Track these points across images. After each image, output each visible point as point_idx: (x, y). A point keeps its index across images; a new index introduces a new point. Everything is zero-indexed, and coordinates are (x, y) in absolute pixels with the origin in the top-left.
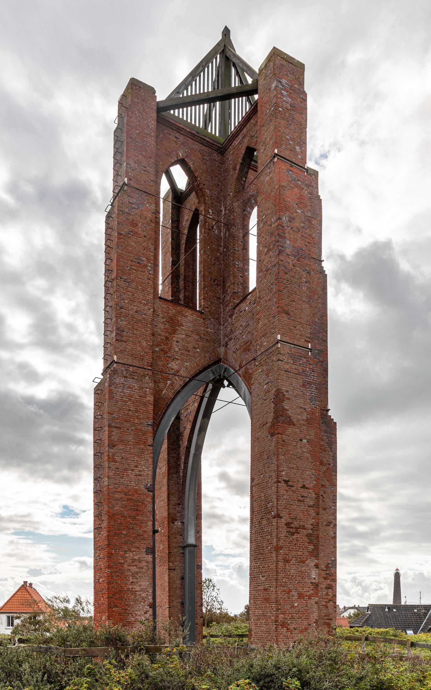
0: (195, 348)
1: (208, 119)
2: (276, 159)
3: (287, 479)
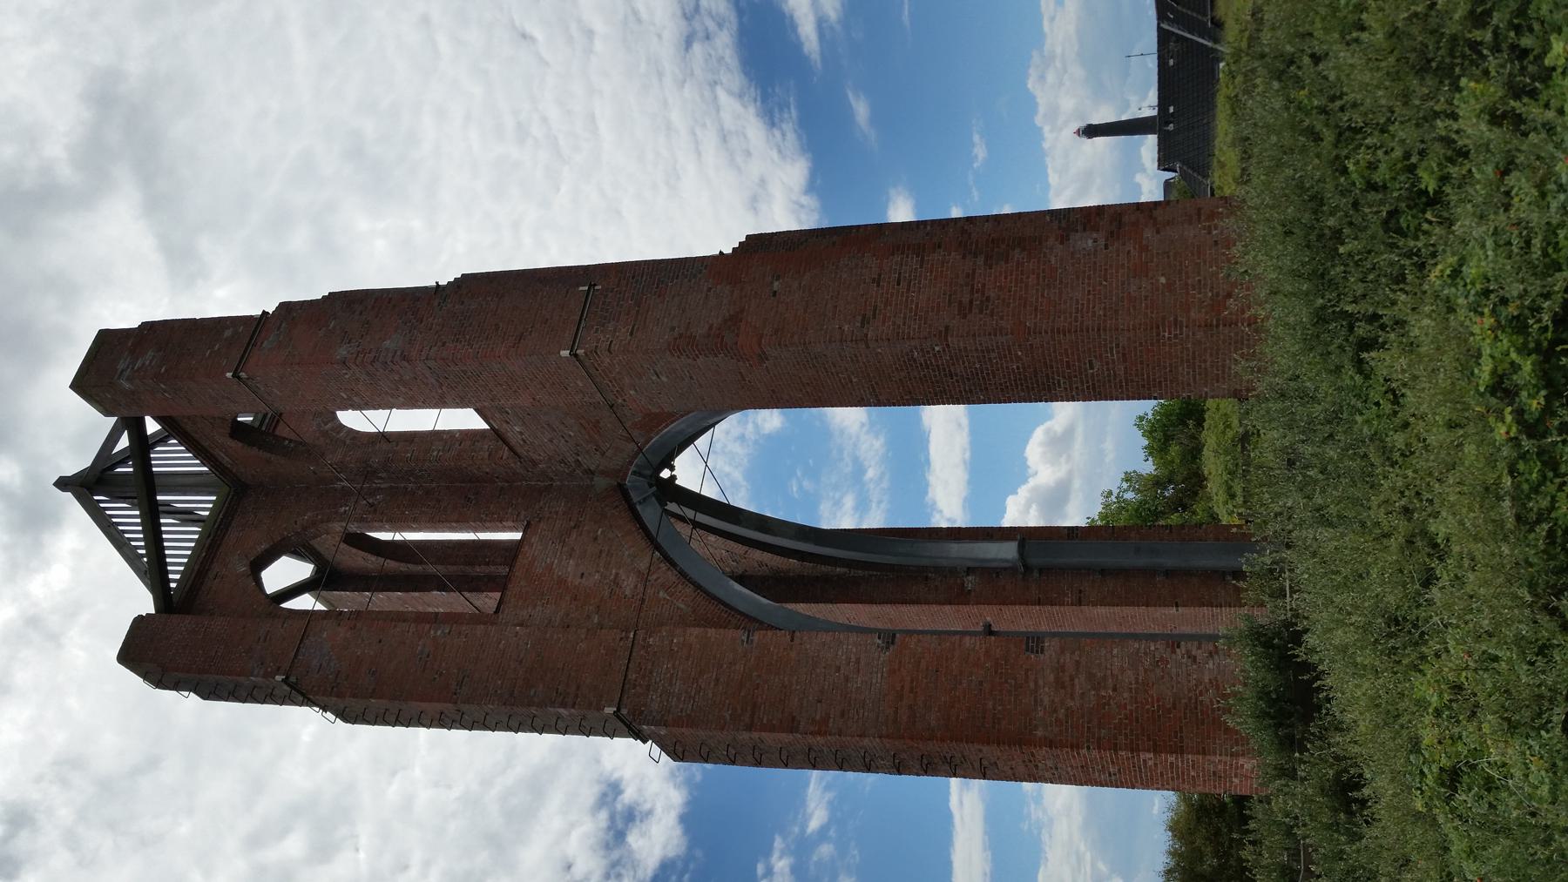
0: (596, 539)
1: (187, 516)
2: (243, 375)
3: (859, 318)
